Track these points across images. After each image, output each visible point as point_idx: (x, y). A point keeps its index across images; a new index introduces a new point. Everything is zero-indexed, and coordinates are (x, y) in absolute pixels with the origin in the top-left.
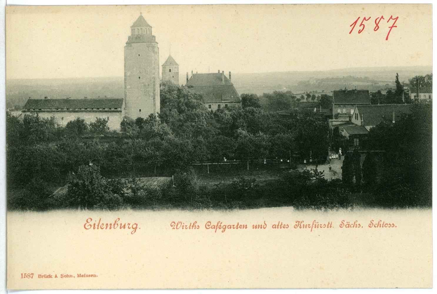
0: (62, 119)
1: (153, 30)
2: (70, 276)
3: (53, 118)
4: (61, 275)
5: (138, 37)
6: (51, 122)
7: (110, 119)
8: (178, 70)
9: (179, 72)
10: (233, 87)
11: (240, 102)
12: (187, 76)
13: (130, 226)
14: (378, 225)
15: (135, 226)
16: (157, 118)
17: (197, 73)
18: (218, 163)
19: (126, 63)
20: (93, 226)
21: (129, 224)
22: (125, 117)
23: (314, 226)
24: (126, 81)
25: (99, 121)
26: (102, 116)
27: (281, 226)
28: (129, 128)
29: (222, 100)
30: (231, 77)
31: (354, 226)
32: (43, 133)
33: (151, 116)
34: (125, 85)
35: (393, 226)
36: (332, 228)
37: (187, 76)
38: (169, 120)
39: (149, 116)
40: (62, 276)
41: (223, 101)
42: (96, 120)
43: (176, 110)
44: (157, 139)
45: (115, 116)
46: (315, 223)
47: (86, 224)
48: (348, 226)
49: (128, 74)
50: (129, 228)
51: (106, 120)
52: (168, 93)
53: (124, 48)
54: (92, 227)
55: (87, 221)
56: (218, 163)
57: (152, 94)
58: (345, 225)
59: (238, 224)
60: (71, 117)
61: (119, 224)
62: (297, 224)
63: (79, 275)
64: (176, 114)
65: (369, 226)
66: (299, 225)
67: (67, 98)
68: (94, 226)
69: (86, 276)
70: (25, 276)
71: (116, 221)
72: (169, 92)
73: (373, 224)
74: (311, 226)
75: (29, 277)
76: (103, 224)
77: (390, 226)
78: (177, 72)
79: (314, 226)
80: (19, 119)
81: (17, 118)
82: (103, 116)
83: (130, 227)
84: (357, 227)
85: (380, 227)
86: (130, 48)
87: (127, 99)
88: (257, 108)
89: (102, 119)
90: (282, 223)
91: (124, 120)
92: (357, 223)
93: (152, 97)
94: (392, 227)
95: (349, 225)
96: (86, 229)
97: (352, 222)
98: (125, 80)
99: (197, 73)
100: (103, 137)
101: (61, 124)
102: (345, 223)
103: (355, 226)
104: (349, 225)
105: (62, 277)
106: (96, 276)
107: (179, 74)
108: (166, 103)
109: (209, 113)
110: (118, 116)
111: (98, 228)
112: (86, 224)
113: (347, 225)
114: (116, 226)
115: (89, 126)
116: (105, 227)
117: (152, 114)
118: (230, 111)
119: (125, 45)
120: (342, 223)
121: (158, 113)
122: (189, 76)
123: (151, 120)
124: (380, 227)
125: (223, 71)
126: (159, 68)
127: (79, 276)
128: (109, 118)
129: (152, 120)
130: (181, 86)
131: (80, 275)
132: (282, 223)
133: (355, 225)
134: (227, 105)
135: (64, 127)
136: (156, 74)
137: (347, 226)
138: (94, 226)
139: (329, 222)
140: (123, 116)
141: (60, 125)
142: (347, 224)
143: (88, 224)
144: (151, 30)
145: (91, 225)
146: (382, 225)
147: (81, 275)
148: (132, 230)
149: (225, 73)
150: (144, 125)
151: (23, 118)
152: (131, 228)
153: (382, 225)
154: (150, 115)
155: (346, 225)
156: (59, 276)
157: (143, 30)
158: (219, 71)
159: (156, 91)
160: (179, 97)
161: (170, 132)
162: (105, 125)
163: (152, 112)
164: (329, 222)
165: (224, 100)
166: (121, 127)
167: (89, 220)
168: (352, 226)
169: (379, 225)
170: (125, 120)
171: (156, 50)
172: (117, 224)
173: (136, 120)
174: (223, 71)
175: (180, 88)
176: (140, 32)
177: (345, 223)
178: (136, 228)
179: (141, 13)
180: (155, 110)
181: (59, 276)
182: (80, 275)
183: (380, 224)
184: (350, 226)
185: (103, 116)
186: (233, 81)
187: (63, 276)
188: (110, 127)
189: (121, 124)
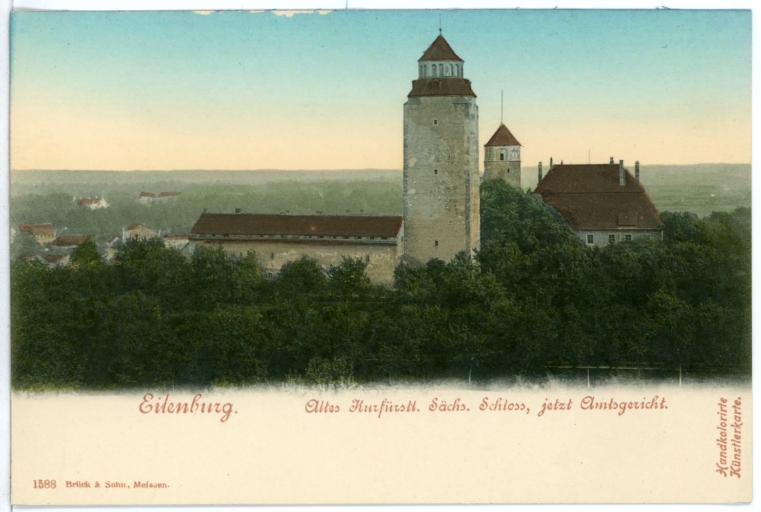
0: (272, 256)
1: (466, 67)
2: (122, 487)
3: (251, 255)
5: (434, 82)
6: (249, 264)
7: (372, 260)
8: (519, 156)
9: (521, 159)
10: (645, 196)
11: (660, 231)
12: (540, 170)
13: (220, 408)
16: (474, 261)
18: (611, 367)
19: (406, 139)
22: (404, 257)
23: (384, 407)
24: (407, 179)
25: (348, 263)
26: (355, 253)
27: (326, 408)
28: (413, 282)
29: (618, 225)
30: (640, 174)
31: (652, 406)
32: (232, 286)
33: (461, 256)
34: (405, 187)
35: (522, 407)
36: (416, 410)
37: (540, 170)
38: (500, 268)
39: (456, 255)
40: (108, 485)
41: (620, 228)
42: (342, 260)
43: (514, 244)
44: (473, 309)
45: (382, 255)
47: (143, 403)
48: (444, 408)
49: (411, 164)
50: (217, 411)
51: (364, 261)
52: (498, 207)
53: (404, 107)
54: (154, 408)
56: (611, 367)
57: (463, 208)
58: (439, 406)
59: (557, 402)
60: (291, 255)
62: (355, 404)
63: (137, 483)
64: (515, 254)
66: (359, 407)
70: (41, 485)
72: (500, 205)
73: (487, 405)
74: (379, 407)
78: (516, 160)
79: (385, 410)
80: (184, 254)
81: (179, 252)
82: (357, 254)
84: (460, 410)
85: (500, 409)
86: (415, 106)
87: (409, 217)
88: (700, 244)
89: (355, 260)
90: (328, 402)
91: (402, 264)
92: (460, 403)
93: (462, 214)
94: (522, 409)
95: (445, 406)
97: (450, 402)
98: (404, 176)
100: (356, 298)
101: (269, 267)
102: (439, 403)
103: (498, 408)
104: (445, 406)
107: (522, 165)
108: (492, 227)
109: (591, 255)
110: (389, 255)
112: (143, 403)
113: (442, 406)
114: (195, 406)
115: (328, 274)
117: (463, 253)
118: (637, 250)
119: (407, 100)
120: (432, 403)
121: (475, 250)
122: (543, 171)
123: (459, 265)
124: (500, 409)
125: (621, 162)
126: (477, 151)
127: (137, 485)
128: (370, 258)
129: (463, 266)
130: (525, 192)
131: (139, 483)
132: (328, 402)
133: (456, 407)
134: (630, 236)
135: (274, 273)
136: (472, 163)
137: (442, 408)
139: (410, 402)
140: (400, 254)
141: (266, 269)
142: (442, 404)
144: (462, 66)
145: (151, 406)
146: (502, 407)
147: (141, 484)
148: (222, 414)
149: (626, 165)
150: (444, 275)
151: (192, 252)
153: (502, 407)
154: (458, 254)
155: (440, 407)
156: (103, 485)
157: (444, 67)
158: (612, 158)
159: (472, 203)
160: (521, 216)
161: (502, 292)
162: (362, 275)
163: (464, 249)
164: (410, 402)
165: (623, 226)
166: (396, 277)
168: (451, 408)
170: (405, 263)
171: (472, 111)
172: (197, 405)
173: (427, 264)
174: (621, 162)
175: (524, 196)
176: (438, 72)
177: (439, 403)
178: (230, 411)
179: (440, 30)
180: (468, 243)
181: (103, 485)
182: (139, 483)
183: (500, 405)
184: (447, 407)
185: (357, 254)
186: (643, 180)
187: (109, 485)
188: (372, 278)
189: (395, 272)
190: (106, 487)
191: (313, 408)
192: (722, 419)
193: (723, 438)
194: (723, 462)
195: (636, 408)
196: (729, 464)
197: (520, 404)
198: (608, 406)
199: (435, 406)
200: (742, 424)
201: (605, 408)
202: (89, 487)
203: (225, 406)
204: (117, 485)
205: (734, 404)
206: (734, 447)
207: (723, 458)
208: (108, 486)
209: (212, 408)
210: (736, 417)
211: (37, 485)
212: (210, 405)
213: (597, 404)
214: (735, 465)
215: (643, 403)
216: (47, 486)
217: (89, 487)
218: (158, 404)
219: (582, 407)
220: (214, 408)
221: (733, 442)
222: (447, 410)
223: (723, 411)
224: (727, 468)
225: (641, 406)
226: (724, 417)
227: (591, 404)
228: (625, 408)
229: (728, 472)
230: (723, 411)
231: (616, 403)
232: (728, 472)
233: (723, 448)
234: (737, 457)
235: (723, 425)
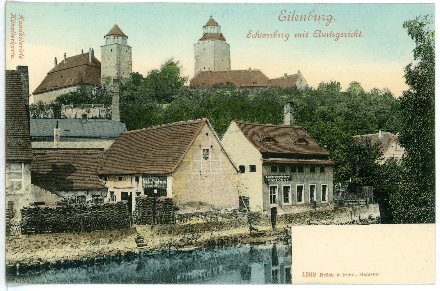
2: (352, 274)
4: (343, 274)
13: (325, 18)
14: (256, 35)
15: (329, 18)
17: (83, 52)
20: (288, 18)
21: (324, 16)
31: (354, 36)
40: (344, 275)
46: (258, 33)
50: (323, 20)
54: (287, 19)
55: (282, 13)
61: (313, 16)
63: (361, 273)
65: (247, 36)
67: (143, 187)
68: (289, 18)
69: (368, 275)
70: (307, 274)
71: (310, 13)
75: (311, 275)
76: (297, 16)
77: (268, 36)
83: (324, 19)
96: (280, 20)
99: (83, 52)
103: (356, 35)
105: (344, 275)
106: (354, 276)
111: (292, 20)
114: (311, 17)
116: (300, 19)
127: (362, 274)
131: (362, 273)
138: (289, 18)
143: (283, 16)
145: (285, 17)
146: (260, 36)
152: (326, 20)
167: (283, 12)
168: (353, 35)
169: (257, 35)
172: (312, 16)
181: (341, 275)
182: (362, 273)
190: (343, 276)
191: (318, 34)
192: (22, 47)
193: (20, 36)
194: (20, 22)
195: (345, 37)
196: (17, 21)
197: (269, 34)
198: (329, 36)
199: (250, 35)
200: (10, 44)
201: (325, 36)
202: (333, 276)
203: (328, 16)
204: (349, 275)
205: (15, 55)
206: (15, 31)
207: (21, 24)
208: (344, 275)
209: (320, 18)
210: (14, 48)
211: (305, 275)
212: (320, 16)
213: (323, 34)
214: (13, 20)
215: (349, 34)
216: (311, 273)
217: (333, 276)
218: (289, 16)
219: (314, 36)
220: (321, 18)
221: (15, 34)
222: (350, 37)
223: (21, 51)
224: (18, 18)
225: (348, 36)
226: (20, 48)
227: (320, 34)
228: (339, 36)
229: (18, 16)
230: (21, 51)
231: (333, 34)
232: (18, 16)
233: (21, 30)
234: (13, 25)
235: (21, 43)
